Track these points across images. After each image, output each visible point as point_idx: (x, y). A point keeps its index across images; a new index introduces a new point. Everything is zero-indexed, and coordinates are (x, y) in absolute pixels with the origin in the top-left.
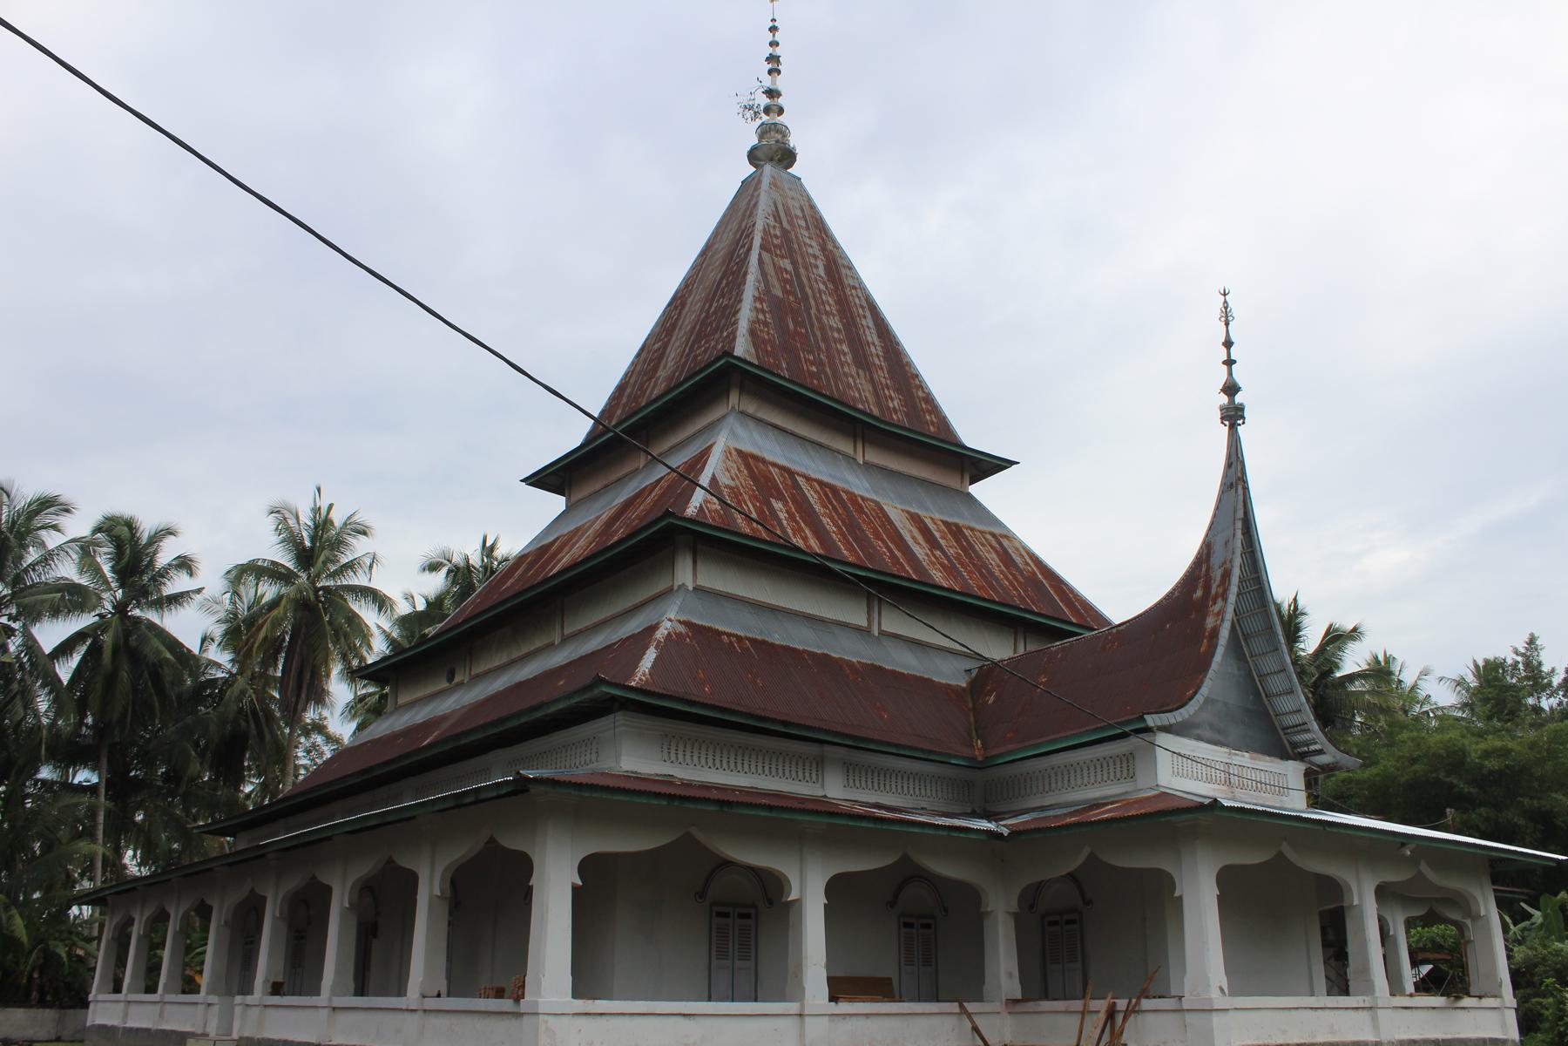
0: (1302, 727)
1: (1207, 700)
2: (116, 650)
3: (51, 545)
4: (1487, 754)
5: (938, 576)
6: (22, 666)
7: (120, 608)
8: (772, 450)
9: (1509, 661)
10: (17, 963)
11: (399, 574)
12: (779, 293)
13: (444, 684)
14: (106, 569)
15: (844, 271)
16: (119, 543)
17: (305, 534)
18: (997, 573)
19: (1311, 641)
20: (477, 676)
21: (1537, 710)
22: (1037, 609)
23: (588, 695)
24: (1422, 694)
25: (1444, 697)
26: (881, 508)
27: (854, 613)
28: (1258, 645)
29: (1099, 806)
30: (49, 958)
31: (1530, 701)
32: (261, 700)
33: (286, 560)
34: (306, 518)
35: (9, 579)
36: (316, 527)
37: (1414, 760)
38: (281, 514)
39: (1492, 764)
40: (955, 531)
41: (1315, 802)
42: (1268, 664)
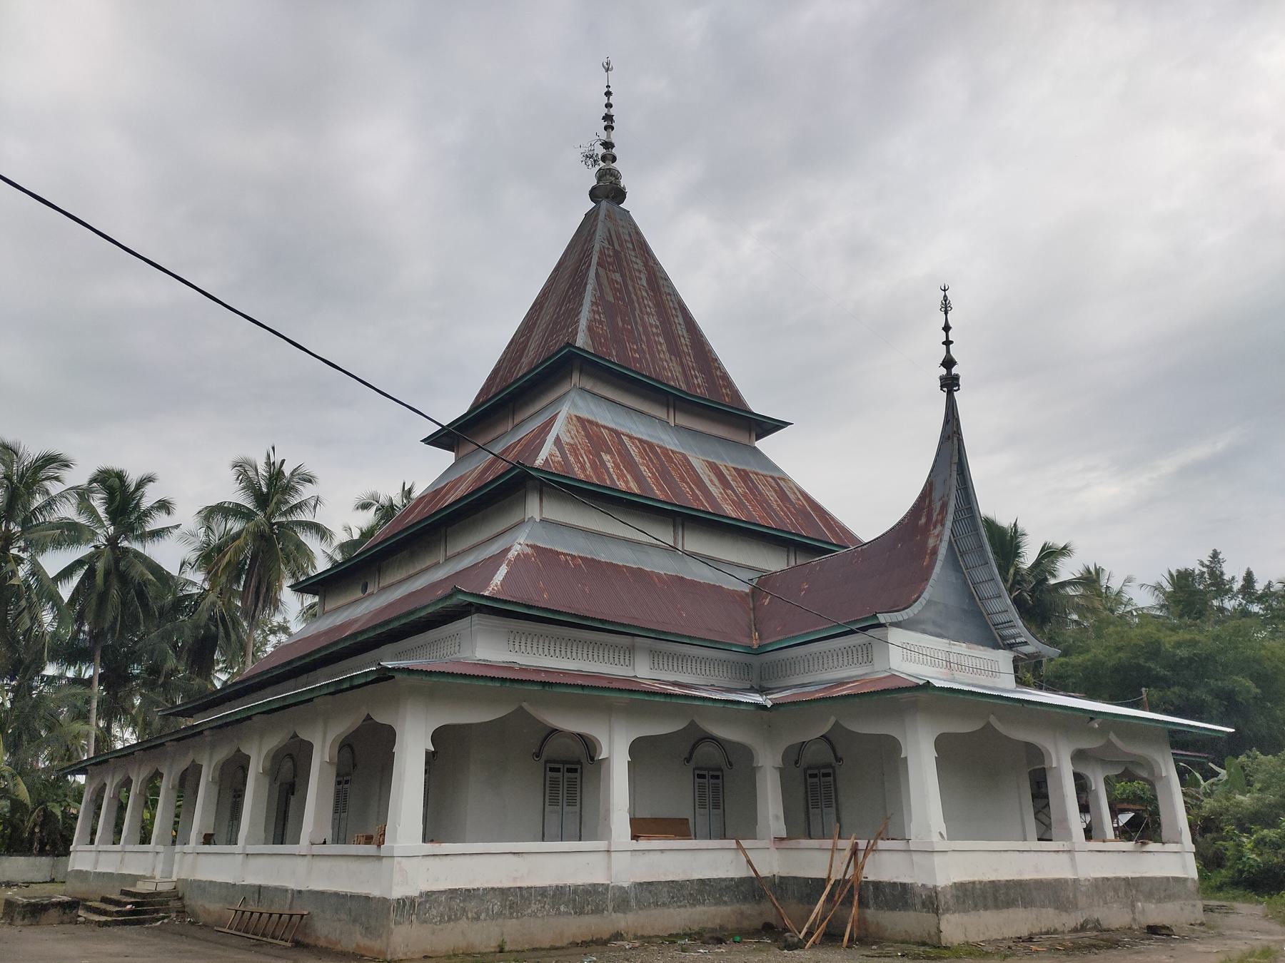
0: (1010, 624)
1: (929, 602)
2: (107, 574)
3: (53, 492)
4: (1179, 645)
5: (729, 510)
6: (29, 587)
7: (112, 541)
8: (605, 417)
9: (1197, 572)
10: (23, 821)
11: (339, 513)
12: (611, 299)
13: (359, 595)
14: (101, 510)
15: (661, 282)
16: (111, 492)
17: (262, 483)
18: (775, 506)
19: (1029, 556)
20: (384, 588)
21: (1221, 609)
22: (804, 534)
23: (449, 602)
24: (1125, 597)
25: (1143, 599)
26: (687, 460)
27: (665, 535)
28: (971, 560)
29: (843, 684)
30: (48, 817)
31: (1215, 603)
32: (229, 610)
33: (249, 504)
34: (262, 469)
35: (19, 520)
36: (271, 476)
37: (1119, 649)
38: (243, 468)
39: (1183, 653)
40: (744, 476)
41: (1020, 682)
42: (979, 574)
